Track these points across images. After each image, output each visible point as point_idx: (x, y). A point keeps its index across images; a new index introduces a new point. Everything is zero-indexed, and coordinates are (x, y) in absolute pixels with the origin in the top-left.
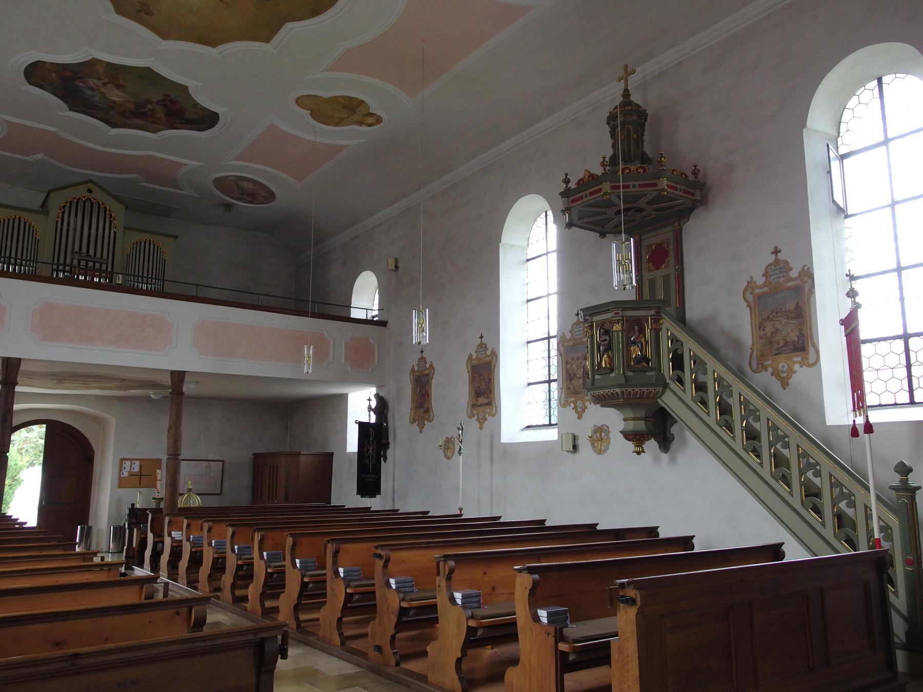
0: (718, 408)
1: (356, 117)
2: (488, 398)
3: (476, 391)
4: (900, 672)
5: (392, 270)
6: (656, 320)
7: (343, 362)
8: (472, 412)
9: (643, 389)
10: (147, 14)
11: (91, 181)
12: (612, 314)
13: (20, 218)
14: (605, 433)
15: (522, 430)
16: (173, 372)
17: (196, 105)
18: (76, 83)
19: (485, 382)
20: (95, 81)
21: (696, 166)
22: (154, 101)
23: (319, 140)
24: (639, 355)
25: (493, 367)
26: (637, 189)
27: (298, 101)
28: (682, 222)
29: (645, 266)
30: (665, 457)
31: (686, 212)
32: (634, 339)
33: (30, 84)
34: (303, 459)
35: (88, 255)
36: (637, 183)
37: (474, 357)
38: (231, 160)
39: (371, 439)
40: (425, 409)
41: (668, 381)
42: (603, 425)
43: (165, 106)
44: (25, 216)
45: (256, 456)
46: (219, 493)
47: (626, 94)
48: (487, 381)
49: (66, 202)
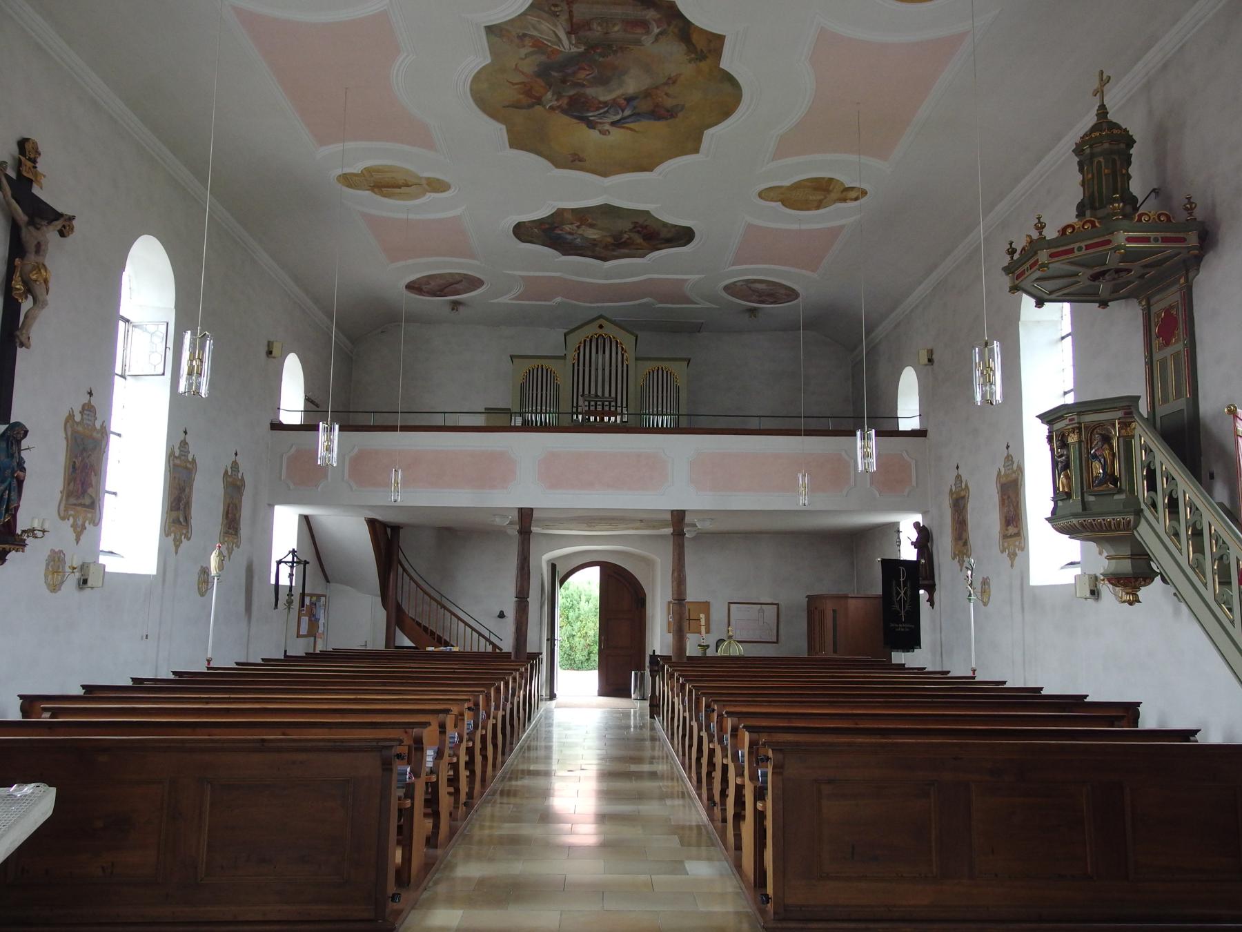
0: (1190, 542)
1: (834, 195)
2: (1017, 526)
3: (1006, 517)
4: (85, 693)
5: (926, 365)
6: (1125, 425)
7: (869, 486)
10: (580, 161)
11: (601, 317)
12: (1067, 422)
13: (542, 366)
15: (1062, 568)
16: (672, 511)
17: (665, 225)
18: (556, 232)
19: (1014, 507)
20: (570, 226)
21: (1190, 198)
22: (627, 230)
23: (804, 227)
24: (1100, 473)
26: (1084, 252)
27: (760, 195)
28: (1191, 275)
29: (1155, 343)
31: (1194, 262)
32: (1095, 452)
33: (523, 242)
34: (852, 604)
35: (596, 396)
36: (1083, 244)
38: (729, 267)
39: (902, 580)
40: (964, 541)
41: (1143, 506)
43: (638, 232)
44: (546, 363)
45: (811, 599)
46: (775, 641)
47: (1103, 111)
48: (1015, 504)
49: (581, 343)
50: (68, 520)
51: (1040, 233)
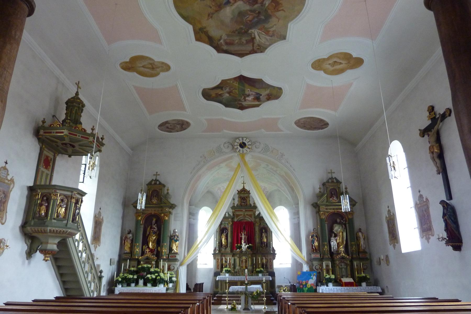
8: (93, 242)
9: (60, 229)
14: (3, 244)
25: (421, 231)
30: (27, 262)
36: (80, 135)
37: (418, 203)
42: (3, 239)
50: (424, 237)
51: (92, 131)
